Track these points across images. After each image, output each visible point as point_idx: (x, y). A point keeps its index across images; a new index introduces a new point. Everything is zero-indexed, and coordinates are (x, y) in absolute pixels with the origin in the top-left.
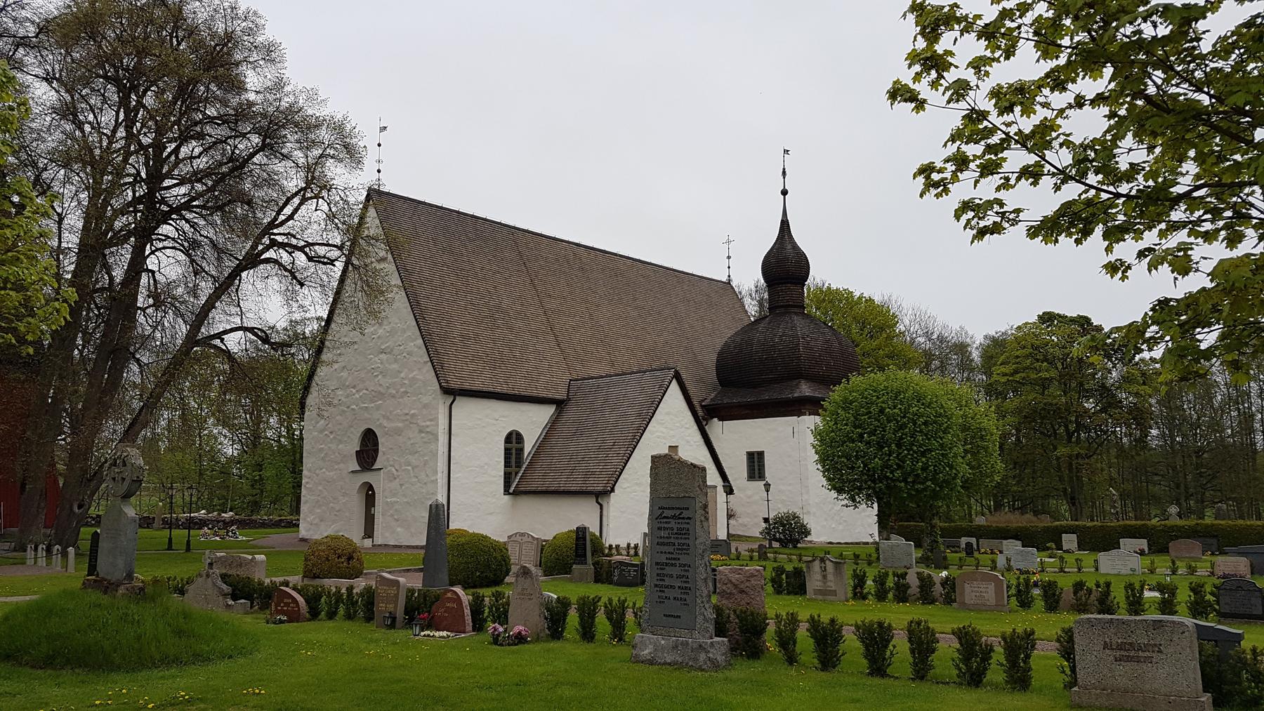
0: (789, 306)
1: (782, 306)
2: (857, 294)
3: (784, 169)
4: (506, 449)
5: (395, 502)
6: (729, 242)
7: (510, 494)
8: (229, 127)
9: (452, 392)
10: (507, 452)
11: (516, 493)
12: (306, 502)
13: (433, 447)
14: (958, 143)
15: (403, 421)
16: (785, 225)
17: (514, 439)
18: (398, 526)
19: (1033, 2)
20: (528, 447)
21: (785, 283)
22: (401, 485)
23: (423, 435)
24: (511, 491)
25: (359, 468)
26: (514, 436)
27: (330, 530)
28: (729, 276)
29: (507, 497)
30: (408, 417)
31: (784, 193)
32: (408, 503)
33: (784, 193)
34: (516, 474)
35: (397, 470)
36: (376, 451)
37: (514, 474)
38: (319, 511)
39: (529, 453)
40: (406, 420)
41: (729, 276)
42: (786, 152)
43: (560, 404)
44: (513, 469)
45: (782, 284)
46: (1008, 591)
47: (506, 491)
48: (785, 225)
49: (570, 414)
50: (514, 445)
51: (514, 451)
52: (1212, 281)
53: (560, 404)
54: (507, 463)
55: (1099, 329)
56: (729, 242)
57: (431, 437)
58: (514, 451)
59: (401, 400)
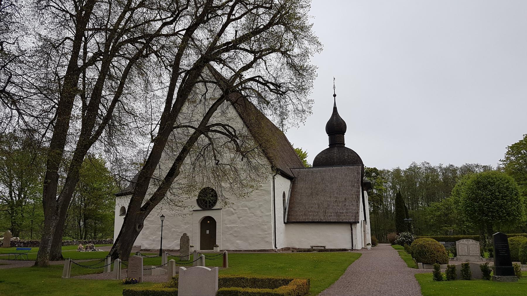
1: (339, 144)
5: (234, 227)
8: (65, 18)
16: (335, 109)
18: (237, 240)
19: (1, 148)
21: (340, 134)
22: (239, 218)
25: (199, 208)
27: (173, 243)
31: (335, 96)
32: (246, 227)
33: (335, 96)
35: (234, 210)
42: (334, 78)
45: (338, 134)
46: (21, 247)
47: (284, 223)
48: (335, 109)
55: (378, 170)
57: (264, 192)
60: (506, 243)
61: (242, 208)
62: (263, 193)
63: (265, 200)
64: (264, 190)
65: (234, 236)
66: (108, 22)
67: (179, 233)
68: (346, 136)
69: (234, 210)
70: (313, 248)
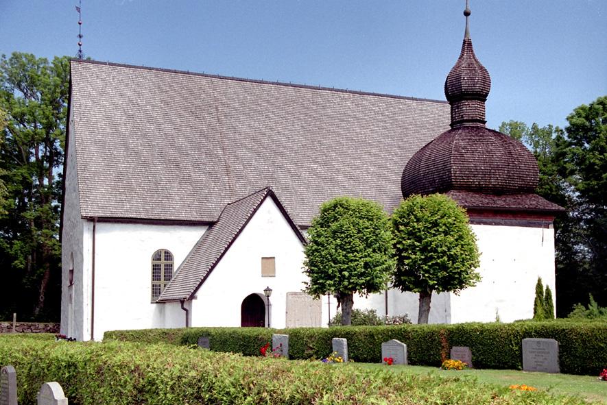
10: (156, 268)
16: (467, 45)
20: (177, 263)
26: (163, 255)
34: (165, 286)
37: (162, 286)
43: (210, 224)
44: (162, 282)
47: (288, 294)
48: (467, 45)
49: (216, 228)
51: (163, 268)
58: (163, 268)
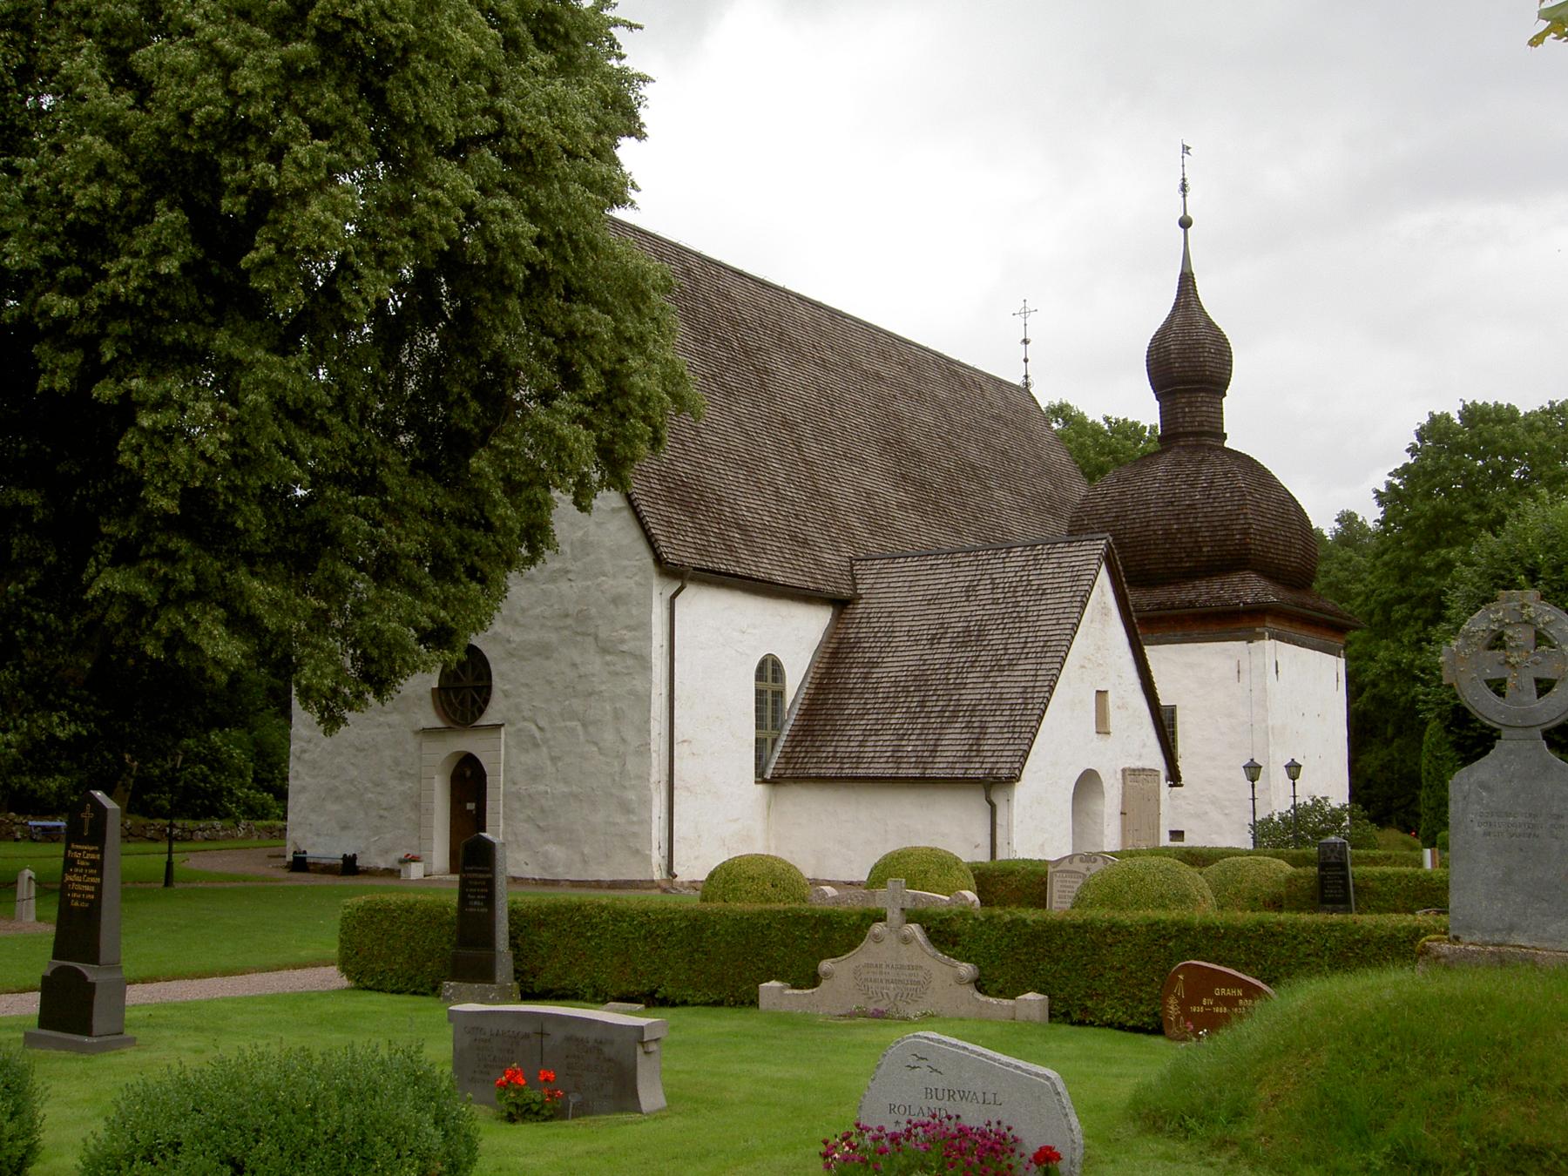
0: (1203, 434)
2: (1491, 404)
3: (1184, 179)
4: (760, 694)
6: (1025, 313)
7: (765, 781)
9: (677, 573)
11: (775, 781)
12: (303, 789)
13: (638, 684)
14: (374, 306)
15: (558, 629)
16: (1187, 282)
17: (769, 670)
23: (608, 658)
24: (768, 776)
25: (438, 723)
28: (1026, 377)
29: (760, 787)
30: (569, 621)
33: (1185, 223)
35: (541, 729)
36: (488, 689)
38: (335, 807)
39: (794, 701)
40: (566, 628)
41: (1026, 377)
42: (1186, 149)
47: (760, 777)
48: (1187, 282)
50: (769, 685)
52: (1412, 456)
53: (841, 605)
54: (760, 723)
56: (1025, 313)
57: (630, 662)
59: (551, 586)
60: (1342, 870)
61: (563, 724)
62: (627, 667)
63: (632, 692)
64: (631, 653)
65: (539, 827)
66: (488, 21)
67: (385, 809)
68: (1232, 405)
69: (541, 729)
70: (97, 848)
